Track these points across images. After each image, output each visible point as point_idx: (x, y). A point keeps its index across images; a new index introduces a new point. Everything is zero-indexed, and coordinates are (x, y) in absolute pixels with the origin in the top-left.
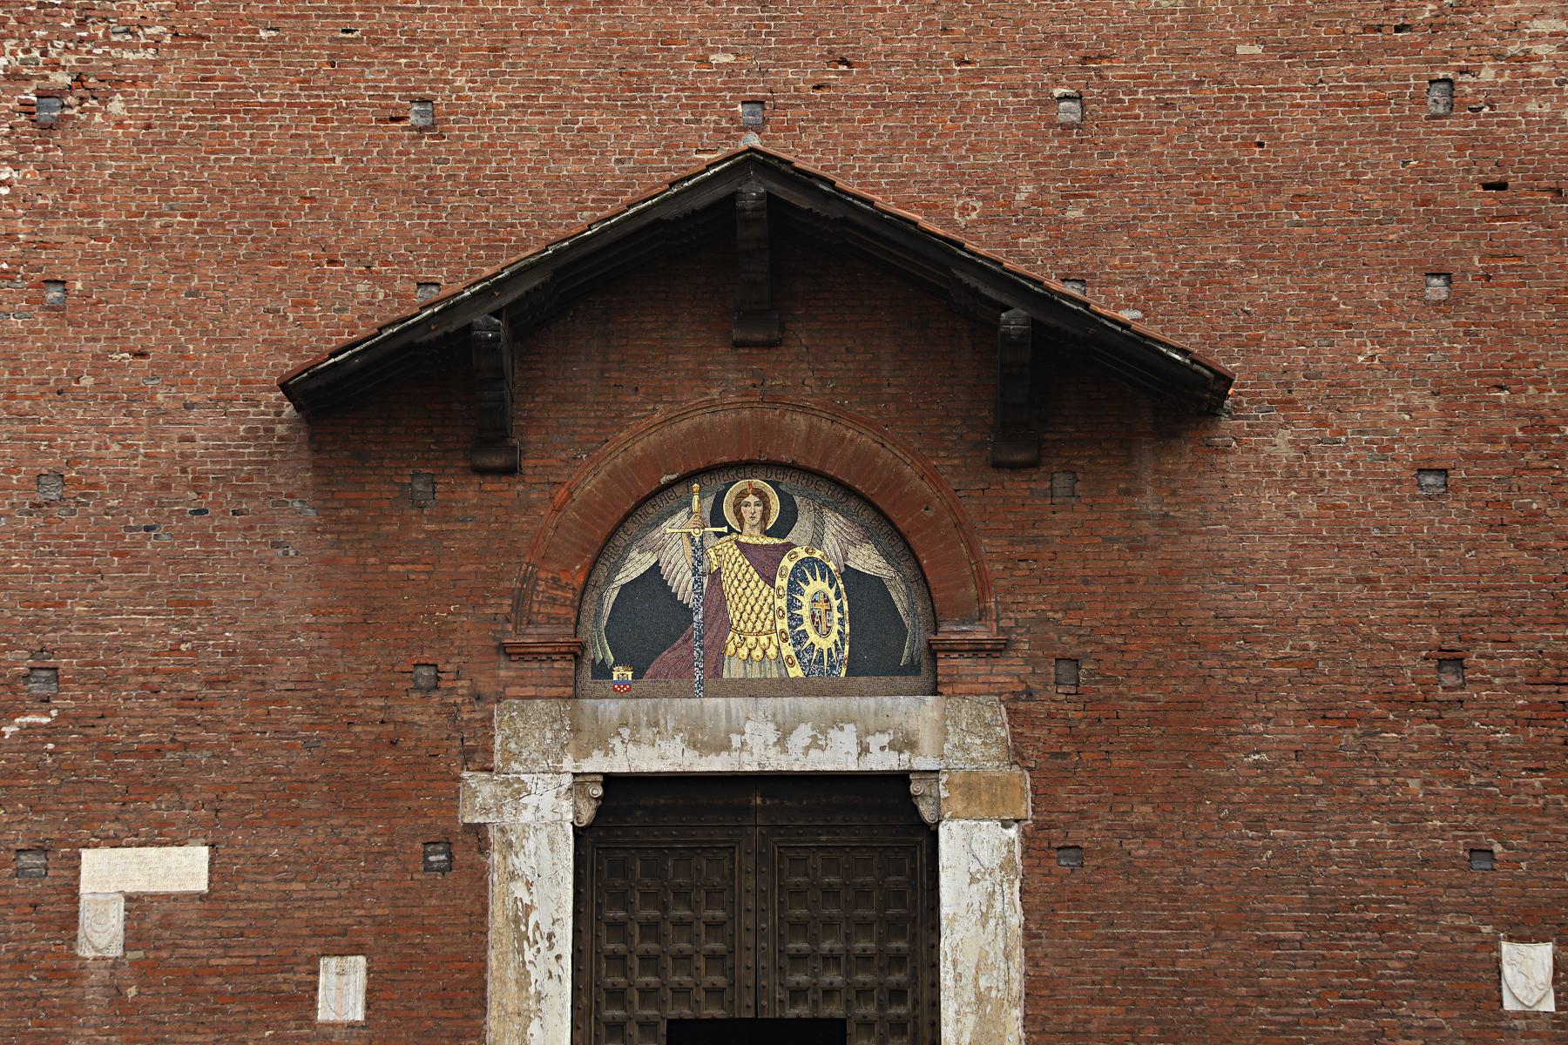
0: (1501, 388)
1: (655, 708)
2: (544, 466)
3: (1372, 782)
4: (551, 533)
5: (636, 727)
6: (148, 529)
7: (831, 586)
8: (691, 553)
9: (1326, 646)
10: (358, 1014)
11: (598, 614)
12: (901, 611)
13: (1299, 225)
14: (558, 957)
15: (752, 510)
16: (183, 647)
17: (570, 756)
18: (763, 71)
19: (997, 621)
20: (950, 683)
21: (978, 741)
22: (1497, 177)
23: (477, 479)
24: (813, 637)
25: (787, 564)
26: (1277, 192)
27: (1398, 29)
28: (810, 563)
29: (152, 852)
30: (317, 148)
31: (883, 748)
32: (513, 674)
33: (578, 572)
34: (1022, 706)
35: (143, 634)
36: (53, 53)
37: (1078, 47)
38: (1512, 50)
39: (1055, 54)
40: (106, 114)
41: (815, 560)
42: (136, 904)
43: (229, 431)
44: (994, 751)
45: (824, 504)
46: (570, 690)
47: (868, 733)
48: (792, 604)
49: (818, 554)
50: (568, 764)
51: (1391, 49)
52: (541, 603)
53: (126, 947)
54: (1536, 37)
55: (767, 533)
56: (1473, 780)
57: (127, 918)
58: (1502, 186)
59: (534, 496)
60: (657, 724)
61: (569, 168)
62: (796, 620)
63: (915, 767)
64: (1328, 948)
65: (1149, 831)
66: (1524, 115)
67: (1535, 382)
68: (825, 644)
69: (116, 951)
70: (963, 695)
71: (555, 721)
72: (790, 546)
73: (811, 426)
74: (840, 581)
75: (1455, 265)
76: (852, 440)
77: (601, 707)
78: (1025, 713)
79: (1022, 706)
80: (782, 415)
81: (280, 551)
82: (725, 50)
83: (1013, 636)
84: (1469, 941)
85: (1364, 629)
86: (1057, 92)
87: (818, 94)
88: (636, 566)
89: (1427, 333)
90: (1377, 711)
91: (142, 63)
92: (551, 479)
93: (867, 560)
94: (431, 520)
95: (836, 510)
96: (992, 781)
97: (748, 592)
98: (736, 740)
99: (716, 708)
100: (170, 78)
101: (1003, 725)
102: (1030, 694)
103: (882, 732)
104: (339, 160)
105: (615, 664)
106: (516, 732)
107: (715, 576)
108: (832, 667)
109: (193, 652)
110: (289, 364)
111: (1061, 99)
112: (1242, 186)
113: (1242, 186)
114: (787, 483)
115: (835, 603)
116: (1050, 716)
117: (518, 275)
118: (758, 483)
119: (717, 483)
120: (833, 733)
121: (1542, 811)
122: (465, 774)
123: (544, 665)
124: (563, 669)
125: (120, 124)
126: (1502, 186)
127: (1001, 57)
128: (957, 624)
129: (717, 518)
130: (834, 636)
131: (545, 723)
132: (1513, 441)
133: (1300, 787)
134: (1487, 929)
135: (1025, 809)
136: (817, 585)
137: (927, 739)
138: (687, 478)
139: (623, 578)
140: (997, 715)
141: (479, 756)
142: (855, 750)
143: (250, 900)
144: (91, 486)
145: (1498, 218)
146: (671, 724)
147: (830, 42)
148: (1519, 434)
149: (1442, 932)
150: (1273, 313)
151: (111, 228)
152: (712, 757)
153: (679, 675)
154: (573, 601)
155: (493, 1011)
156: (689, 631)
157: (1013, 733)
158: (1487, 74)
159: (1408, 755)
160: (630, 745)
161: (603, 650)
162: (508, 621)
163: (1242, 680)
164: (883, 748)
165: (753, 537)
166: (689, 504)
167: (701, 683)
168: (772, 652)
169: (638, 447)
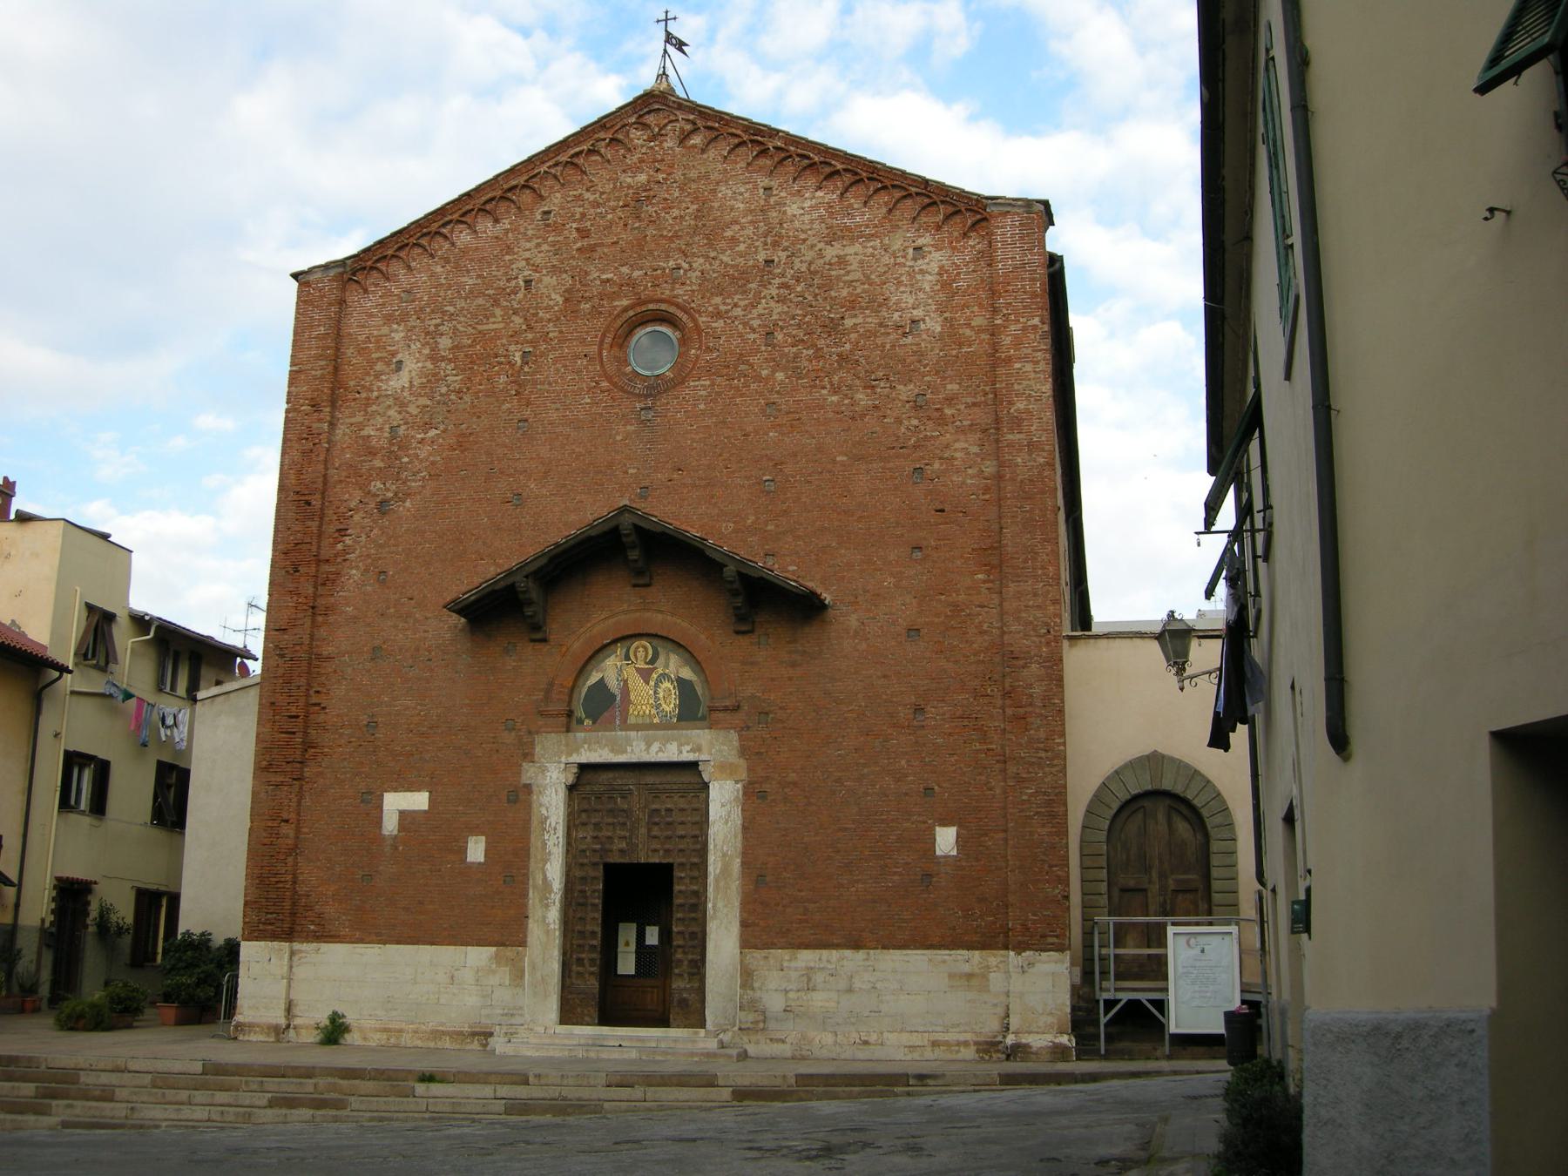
0: (942, 594)
3: (886, 761)
9: (869, 705)
11: (579, 699)
12: (699, 694)
13: (861, 529)
14: (558, 838)
15: (641, 653)
16: (422, 713)
23: (532, 644)
25: (655, 676)
26: (852, 516)
27: (901, 448)
29: (409, 794)
36: (388, 485)
37: (773, 460)
38: (946, 455)
40: (404, 507)
42: (403, 814)
43: (441, 628)
46: (564, 729)
48: (655, 693)
50: (563, 759)
53: (399, 831)
54: (955, 450)
55: (647, 663)
56: (927, 760)
57: (399, 820)
64: (866, 831)
65: (795, 784)
66: (952, 481)
69: (395, 832)
70: (721, 729)
81: (457, 675)
82: (634, 468)
84: (923, 826)
86: (765, 478)
87: (669, 483)
88: (594, 678)
90: (889, 731)
93: (687, 673)
94: (514, 661)
96: (731, 764)
98: (629, 749)
100: (427, 492)
102: (748, 728)
103: (688, 744)
104: (486, 519)
107: (626, 681)
108: (671, 718)
109: (425, 715)
111: (766, 481)
112: (839, 514)
113: (839, 514)
114: (656, 642)
115: (673, 692)
116: (755, 737)
118: (644, 643)
119: (627, 643)
120: (668, 746)
121: (954, 772)
122: (524, 764)
125: (408, 511)
127: (742, 465)
129: (627, 658)
130: (672, 705)
132: (947, 616)
134: (930, 822)
135: (744, 776)
136: (667, 685)
137: (705, 748)
138: (615, 641)
139: (589, 683)
140: (733, 735)
141: (528, 756)
143: (443, 813)
144: (392, 651)
145: (940, 524)
146: (604, 742)
147: (675, 462)
148: (949, 613)
149: (913, 823)
151: (403, 550)
155: (532, 860)
158: (936, 466)
159: (901, 750)
163: (834, 720)
165: (641, 665)
167: (619, 726)
168: (647, 712)
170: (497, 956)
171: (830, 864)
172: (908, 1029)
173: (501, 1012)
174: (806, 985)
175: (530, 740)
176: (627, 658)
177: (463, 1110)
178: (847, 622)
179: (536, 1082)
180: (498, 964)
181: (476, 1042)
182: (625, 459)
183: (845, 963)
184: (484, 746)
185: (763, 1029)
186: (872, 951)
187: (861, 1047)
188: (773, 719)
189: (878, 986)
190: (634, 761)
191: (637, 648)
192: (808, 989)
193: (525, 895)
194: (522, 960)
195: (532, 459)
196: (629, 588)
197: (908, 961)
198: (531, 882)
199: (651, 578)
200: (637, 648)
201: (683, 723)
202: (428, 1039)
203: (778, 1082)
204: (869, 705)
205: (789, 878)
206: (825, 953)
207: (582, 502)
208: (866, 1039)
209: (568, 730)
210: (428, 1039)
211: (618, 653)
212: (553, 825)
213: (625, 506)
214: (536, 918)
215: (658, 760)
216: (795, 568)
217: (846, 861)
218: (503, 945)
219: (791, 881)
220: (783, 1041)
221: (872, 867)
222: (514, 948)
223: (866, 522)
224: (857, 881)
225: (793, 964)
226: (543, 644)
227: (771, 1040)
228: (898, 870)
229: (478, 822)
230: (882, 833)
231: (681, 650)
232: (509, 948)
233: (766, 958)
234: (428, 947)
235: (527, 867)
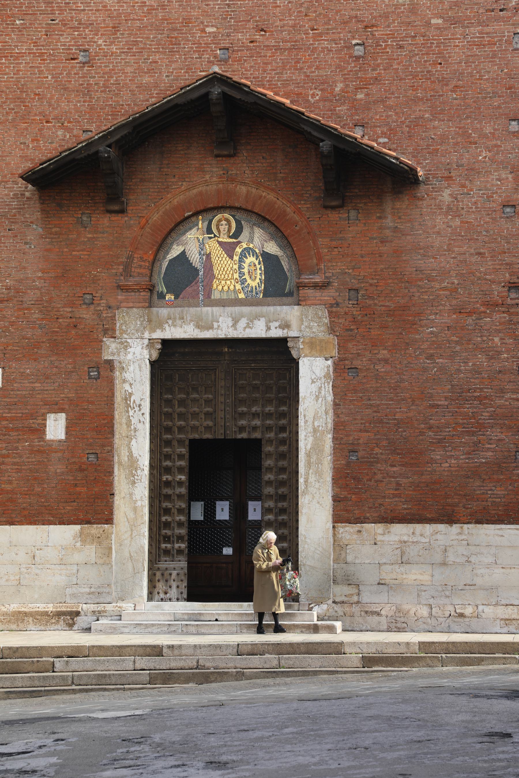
1: (182, 312)
2: (136, 209)
3: (479, 339)
4: (139, 238)
5: (175, 319)
7: (257, 259)
8: (198, 246)
10: (62, 436)
11: (160, 272)
12: (286, 270)
15: (224, 227)
17: (147, 332)
19: (324, 274)
20: (304, 300)
21: (316, 324)
23: (108, 215)
24: (249, 281)
25: (238, 250)
26: (447, 85)
27: (501, 10)
30: (41, 72)
31: (276, 328)
32: (124, 297)
33: (151, 254)
34: (334, 309)
37: (363, 21)
39: (353, 25)
41: (250, 248)
43: (6, 195)
44: (322, 329)
45: (254, 224)
46: (147, 304)
47: (270, 321)
48: (240, 267)
49: (251, 246)
52: (135, 267)
55: (230, 237)
59: (132, 222)
60: (183, 318)
61: (146, 79)
62: (242, 274)
63: (290, 336)
64: (458, 408)
65: (386, 361)
68: (254, 284)
70: (310, 305)
71: (141, 317)
72: (240, 242)
73: (248, 191)
74: (260, 257)
76: (265, 197)
77: (160, 311)
78: (335, 312)
79: (334, 309)
80: (236, 186)
81: (28, 246)
82: (212, 26)
83: (331, 280)
86: (354, 42)
87: (252, 45)
88: (175, 251)
92: (139, 215)
95: (259, 227)
97: (222, 262)
98: (215, 325)
99: (207, 311)
101: (326, 318)
102: (337, 304)
103: (276, 321)
104: (50, 77)
105: (167, 293)
106: (125, 322)
107: (208, 256)
108: (257, 294)
114: (239, 215)
118: (226, 215)
119: (209, 216)
120: (256, 322)
122: (105, 339)
123: (137, 294)
124: (145, 296)
128: (308, 275)
130: (258, 280)
131: (137, 318)
133: (449, 342)
135: (335, 352)
137: (294, 324)
138: (197, 214)
142: (264, 329)
143: (18, 390)
146: (189, 318)
147: (257, 21)
149: (506, 401)
150: (444, 139)
152: (206, 332)
153: (193, 297)
154: (148, 267)
155: (117, 436)
156: (197, 279)
157: (330, 321)
160: (172, 327)
161: (162, 287)
162: (122, 275)
163: (426, 297)
164: (276, 328)
165: (224, 239)
166: (198, 225)
167: (202, 301)
168: (232, 287)
169: (175, 201)
170: (81, 533)
171: (422, 440)
172: (504, 602)
173: (88, 590)
174: (399, 559)
175: (110, 315)
176: (209, 231)
177: (109, 682)
178: (440, 198)
179: (170, 653)
180: (84, 542)
181: (62, 622)
182: (203, 15)
183: (439, 536)
184: (61, 320)
185: (358, 602)
186: (465, 526)
187: (456, 620)
188: (363, 295)
189: (472, 559)
190: (220, 337)
191: (220, 221)
192: (402, 563)
193: (111, 473)
194: (108, 537)
195: (97, 10)
196: (210, 158)
197: (502, 536)
198: (116, 458)
199: (235, 148)
200: (220, 221)
201: (269, 299)
202: (9, 621)
203: (403, 649)
204: (462, 282)
205: (381, 454)
206: (418, 527)
207: (156, 62)
208: (462, 611)
209: (150, 306)
210: (9, 621)
211: (200, 226)
212: (138, 403)
213: (215, 73)
214: (123, 495)
215: (246, 336)
216: (386, 140)
217: (438, 437)
218: (89, 522)
219: (383, 457)
220: (378, 614)
221: (465, 443)
222: (100, 526)
223: (462, 91)
224: (451, 457)
225: (386, 538)
226: (120, 215)
227: (366, 612)
228: (492, 446)
229: (57, 399)
230: (475, 410)
231: (266, 224)
232: (95, 526)
233: (360, 531)
234: (7, 527)
235: (111, 444)
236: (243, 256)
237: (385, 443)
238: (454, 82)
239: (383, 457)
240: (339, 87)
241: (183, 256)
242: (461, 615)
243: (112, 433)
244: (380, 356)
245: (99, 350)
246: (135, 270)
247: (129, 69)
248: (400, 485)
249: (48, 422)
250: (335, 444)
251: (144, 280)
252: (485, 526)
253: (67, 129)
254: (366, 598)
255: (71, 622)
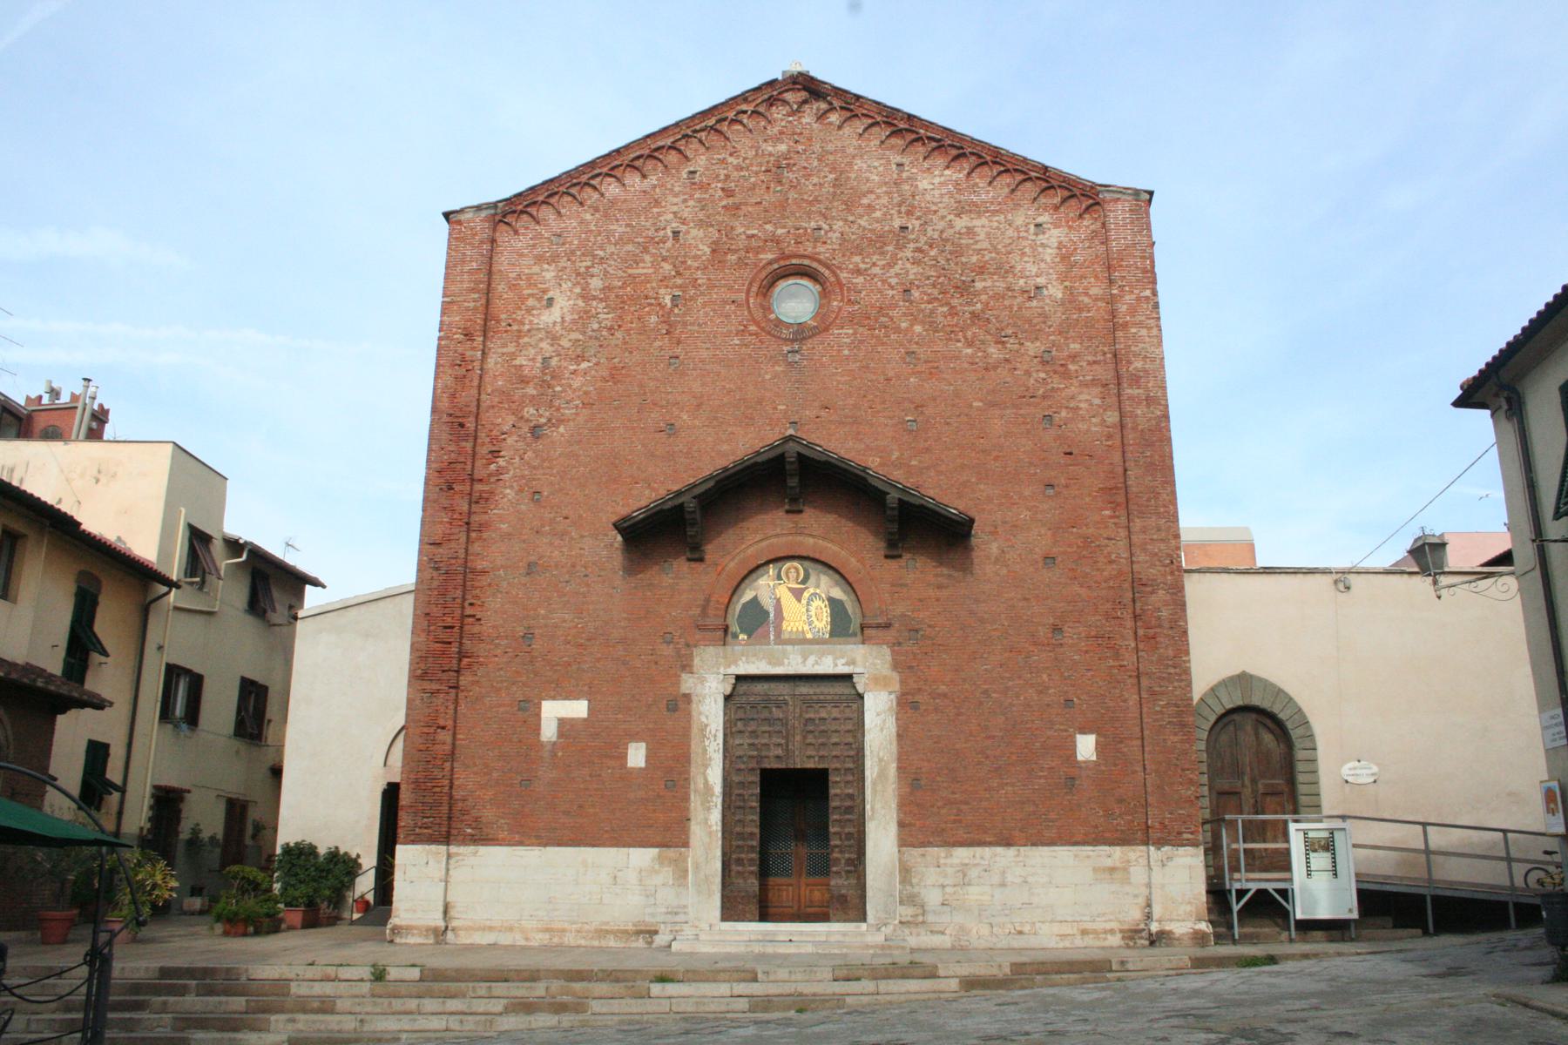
6: (567, 582)
10: (642, 764)
11: (734, 615)
15: (793, 574)
18: (797, 412)
22: (1068, 451)
23: (688, 563)
24: (816, 623)
25: (806, 595)
27: (1031, 397)
28: (815, 594)
29: (567, 703)
30: (632, 442)
35: (565, 621)
38: (1071, 405)
39: (907, 405)
42: (562, 722)
45: (820, 572)
48: (807, 611)
49: (818, 591)
50: (722, 670)
51: (1029, 405)
54: (1080, 401)
56: (1066, 674)
58: (1070, 454)
61: (725, 447)
62: (809, 617)
67: (1086, 525)
75: (1055, 482)
79: (896, 648)
85: (1025, 618)
88: (748, 596)
89: (1046, 506)
91: (572, 414)
93: (837, 593)
98: (786, 661)
100: (581, 419)
110: (614, 518)
117: (706, 480)
120: (823, 659)
122: (683, 675)
126: (1070, 454)
132: (1078, 547)
133: (1002, 678)
135: (897, 687)
137: (859, 659)
141: (687, 667)
150: (990, 499)
151: (558, 472)
170: (660, 857)
172: (1059, 918)
180: (661, 863)
181: (641, 940)
183: (998, 859)
185: (923, 922)
186: (1022, 849)
191: (789, 569)
193: (686, 799)
194: (685, 861)
198: (692, 786)
206: (979, 850)
211: (771, 573)
219: (945, 785)
220: (943, 933)
225: (949, 861)
227: (932, 932)
233: (923, 855)
236: (810, 600)
237: (945, 772)
238: (995, 454)
239: (945, 785)
240: (896, 455)
241: (755, 601)
242: (1020, 933)
243: (689, 761)
244: (939, 691)
245: (677, 683)
246: (711, 612)
247: (710, 439)
248: (961, 811)
249: (629, 751)
250: (899, 773)
251: (720, 622)
252: (1040, 848)
253: (653, 489)
254: (930, 918)
255: (649, 940)
